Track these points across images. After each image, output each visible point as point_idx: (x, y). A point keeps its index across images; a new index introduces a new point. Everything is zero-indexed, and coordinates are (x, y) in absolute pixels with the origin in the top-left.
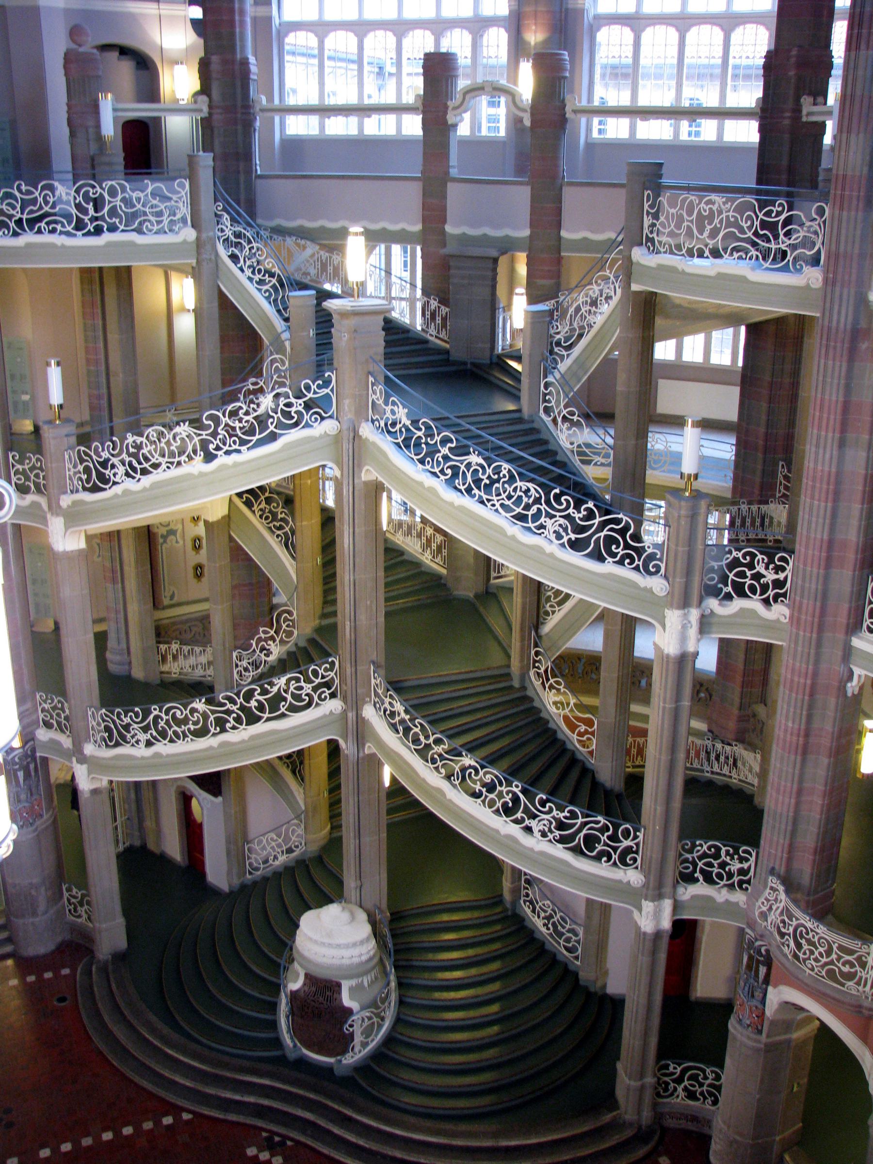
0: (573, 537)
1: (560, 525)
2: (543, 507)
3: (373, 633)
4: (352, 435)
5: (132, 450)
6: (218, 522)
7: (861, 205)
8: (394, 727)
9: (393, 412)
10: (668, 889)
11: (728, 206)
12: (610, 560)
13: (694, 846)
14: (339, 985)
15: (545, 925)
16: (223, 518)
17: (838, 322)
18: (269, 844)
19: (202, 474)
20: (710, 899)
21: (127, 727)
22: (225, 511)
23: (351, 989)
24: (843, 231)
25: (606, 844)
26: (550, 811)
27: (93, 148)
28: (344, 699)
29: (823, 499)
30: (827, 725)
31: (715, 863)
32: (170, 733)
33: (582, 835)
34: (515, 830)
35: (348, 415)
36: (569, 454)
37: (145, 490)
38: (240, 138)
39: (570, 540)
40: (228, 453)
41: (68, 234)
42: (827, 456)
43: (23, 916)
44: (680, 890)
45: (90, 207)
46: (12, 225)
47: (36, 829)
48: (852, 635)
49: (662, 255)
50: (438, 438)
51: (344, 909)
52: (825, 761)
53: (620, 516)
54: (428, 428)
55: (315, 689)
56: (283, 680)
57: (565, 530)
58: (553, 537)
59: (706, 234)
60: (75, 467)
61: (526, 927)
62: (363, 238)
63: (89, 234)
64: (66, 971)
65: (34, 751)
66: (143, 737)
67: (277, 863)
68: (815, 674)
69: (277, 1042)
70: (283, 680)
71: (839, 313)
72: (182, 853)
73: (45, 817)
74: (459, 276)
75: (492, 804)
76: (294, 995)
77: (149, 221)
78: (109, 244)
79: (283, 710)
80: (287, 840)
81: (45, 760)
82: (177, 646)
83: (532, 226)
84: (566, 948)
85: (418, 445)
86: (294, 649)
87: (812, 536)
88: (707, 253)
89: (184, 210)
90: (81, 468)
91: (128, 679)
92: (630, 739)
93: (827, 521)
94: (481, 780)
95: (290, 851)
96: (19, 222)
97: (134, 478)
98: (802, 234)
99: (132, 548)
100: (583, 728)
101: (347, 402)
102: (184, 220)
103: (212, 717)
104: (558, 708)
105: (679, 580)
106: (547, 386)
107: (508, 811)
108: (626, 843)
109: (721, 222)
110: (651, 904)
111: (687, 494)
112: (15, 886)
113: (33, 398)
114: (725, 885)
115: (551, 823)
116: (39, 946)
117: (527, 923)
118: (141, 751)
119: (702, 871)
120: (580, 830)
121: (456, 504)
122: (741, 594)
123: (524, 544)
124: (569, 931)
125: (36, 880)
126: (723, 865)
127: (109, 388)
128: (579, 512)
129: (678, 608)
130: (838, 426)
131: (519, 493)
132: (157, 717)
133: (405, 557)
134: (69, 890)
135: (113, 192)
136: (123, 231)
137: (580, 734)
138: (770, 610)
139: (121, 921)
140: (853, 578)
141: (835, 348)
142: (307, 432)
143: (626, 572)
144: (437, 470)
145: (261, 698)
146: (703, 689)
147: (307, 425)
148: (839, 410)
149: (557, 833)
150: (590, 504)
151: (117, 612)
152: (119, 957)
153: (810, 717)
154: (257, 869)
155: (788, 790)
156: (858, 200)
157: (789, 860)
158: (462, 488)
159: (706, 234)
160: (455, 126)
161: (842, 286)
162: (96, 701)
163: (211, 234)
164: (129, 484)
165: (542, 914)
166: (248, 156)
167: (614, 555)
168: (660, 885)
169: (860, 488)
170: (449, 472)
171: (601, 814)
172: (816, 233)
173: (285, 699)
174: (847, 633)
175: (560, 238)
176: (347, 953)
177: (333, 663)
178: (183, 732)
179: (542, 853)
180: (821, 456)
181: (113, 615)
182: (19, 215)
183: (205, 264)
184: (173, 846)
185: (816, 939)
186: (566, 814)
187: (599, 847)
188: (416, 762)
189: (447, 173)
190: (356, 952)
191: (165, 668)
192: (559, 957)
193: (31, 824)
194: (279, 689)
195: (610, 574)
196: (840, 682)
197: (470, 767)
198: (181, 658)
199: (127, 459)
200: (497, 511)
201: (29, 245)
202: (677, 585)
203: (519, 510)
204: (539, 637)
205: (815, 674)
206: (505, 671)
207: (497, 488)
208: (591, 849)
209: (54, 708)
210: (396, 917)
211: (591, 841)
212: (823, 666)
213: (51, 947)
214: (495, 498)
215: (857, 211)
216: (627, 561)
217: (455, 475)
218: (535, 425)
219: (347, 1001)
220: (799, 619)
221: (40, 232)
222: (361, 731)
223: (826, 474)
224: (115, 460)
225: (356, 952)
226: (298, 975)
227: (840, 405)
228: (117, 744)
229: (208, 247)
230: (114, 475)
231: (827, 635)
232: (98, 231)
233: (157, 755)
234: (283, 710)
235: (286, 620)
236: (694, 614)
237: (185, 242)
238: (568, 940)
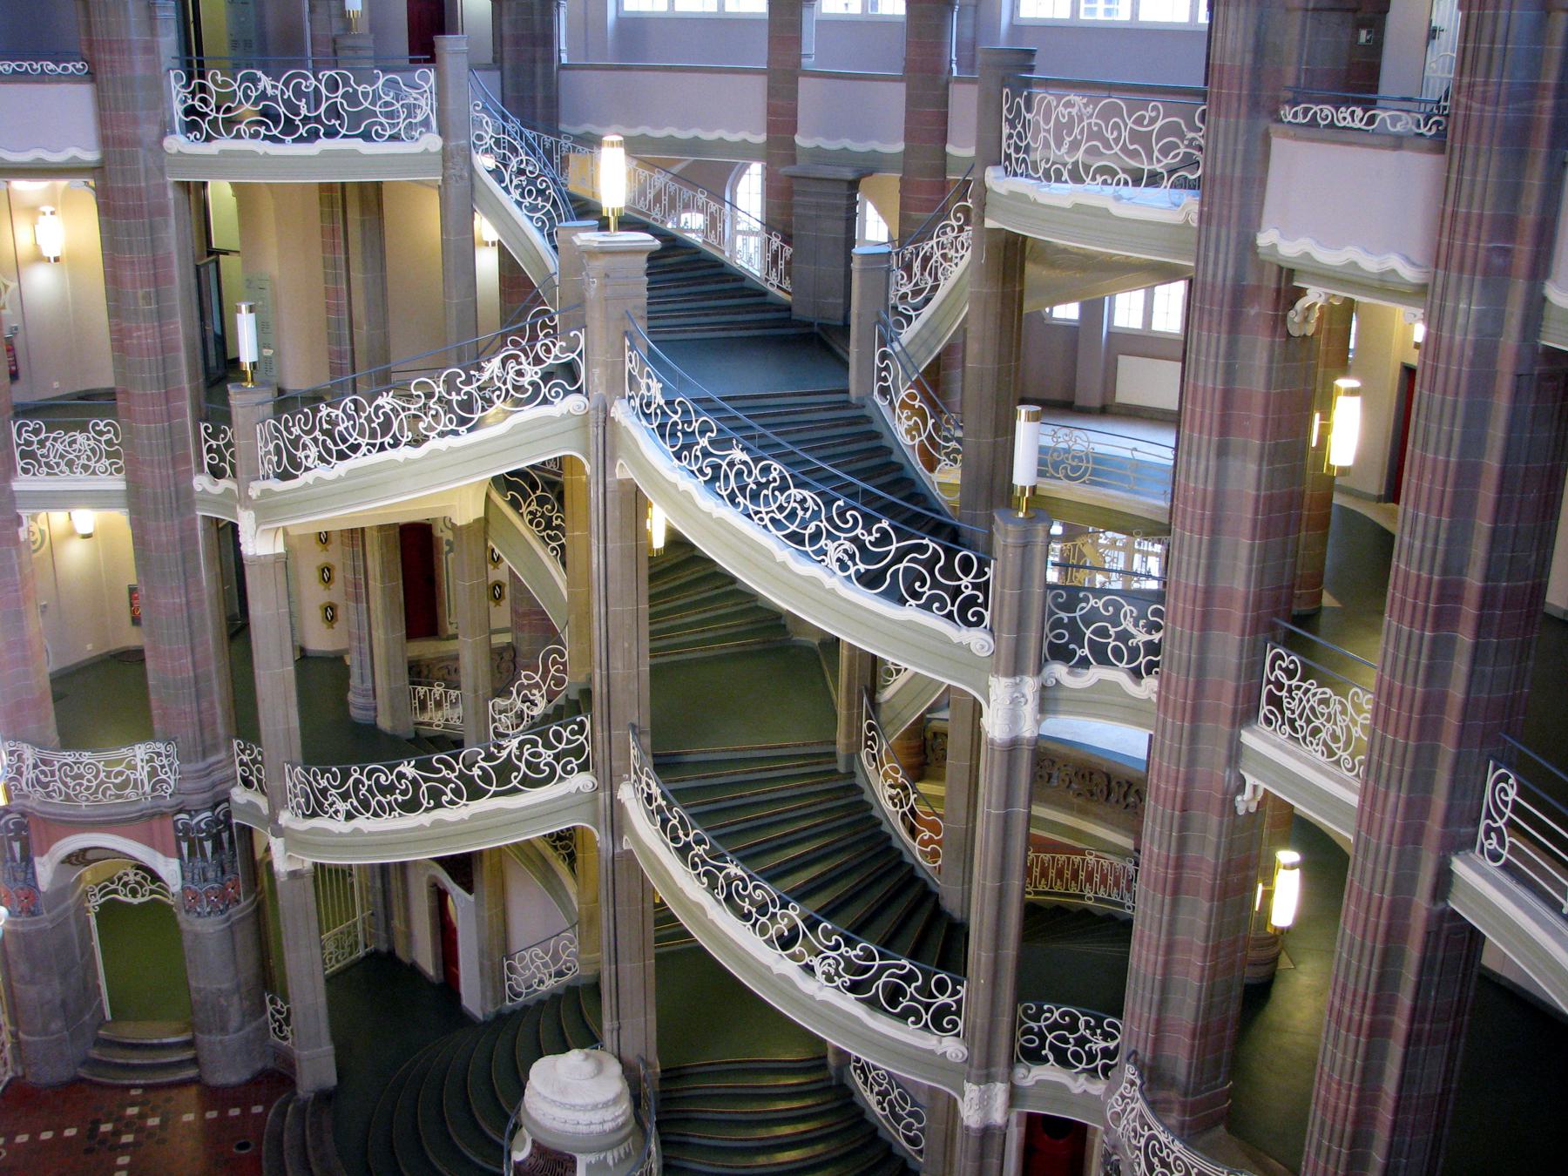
0: (862, 567)
1: (845, 551)
2: (824, 525)
3: (634, 686)
4: (601, 416)
5: (325, 426)
6: (468, 526)
7: (1244, 109)
9: (649, 389)
10: (1000, 1068)
11: (1090, 109)
12: (912, 602)
13: (1040, 1011)
14: (573, 1161)
15: (879, 1103)
16: (477, 521)
17: (1215, 276)
18: (532, 961)
19: (408, 462)
20: (1062, 1087)
21: (324, 792)
22: (479, 512)
23: (589, 1167)
24: (1220, 146)
25: (913, 999)
26: (837, 947)
27: (337, 27)
29: (1196, 528)
30: (1207, 853)
31: (1071, 1037)
32: (374, 803)
33: (880, 982)
34: (790, 968)
35: (598, 390)
36: (908, 452)
37: (339, 479)
38: (537, 18)
39: (858, 571)
40: (442, 434)
41: (274, 139)
42: (1202, 467)
43: (210, 1032)
44: (1020, 1071)
45: (303, 104)
46: (205, 126)
47: (228, 919)
48: (1241, 726)
49: (1019, 179)
50: (696, 425)
51: (587, 1056)
52: (1205, 905)
53: (925, 541)
54: (686, 412)
55: (557, 758)
57: (852, 557)
58: (835, 567)
59: (1064, 149)
60: (266, 445)
61: (854, 1104)
62: (622, 150)
63: (301, 139)
64: (257, 1109)
65: (228, 815)
66: (342, 806)
67: (543, 988)
68: (1189, 781)
71: (1216, 264)
72: (436, 967)
73: (243, 904)
74: (811, 204)
75: (763, 930)
76: (518, 1165)
77: (381, 124)
78: (325, 154)
79: (515, 782)
80: (556, 957)
81: (242, 827)
82: (441, 689)
83: (907, 139)
84: (907, 1138)
85: (673, 435)
86: (562, 703)
87: (1183, 581)
88: (1066, 176)
89: (427, 108)
90: (271, 447)
91: (372, 729)
92: (1031, 855)
93: (1203, 561)
94: (750, 896)
95: (560, 974)
96: (214, 123)
97: (329, 463)
98: (1182, 150)
99: (377, 555)
100: (927, 834)
101: (597, 371)
102: (426, 123)
103: (424, 787)
104: (895, 805)
105: (1007, 636)
106: (884, 356)
107: (786, 942)
108: (942, 999)
109: (1082, 131)
110: (975, 1087)
111: (1021, 515)
112: (199, 991)
113: (278, 354)
114: (1084, 1070)
115: (838, 964)
116: (229, 1074)
117: (856, 1098)
118: (340, 826)
119: (1053, 1047)
120: (878, 976)
121: (715, 515)
122: (1103, 660)
123: (797, 575)
124: (910, 1114)
125: (226, 986)
126: (1081, 1042)
127: (352, 343)
128: (870, 534)
129: (1006, 675)
130: (1216, 425)
131: (793, 504)
132: (357, 782)
133: (737, 586)
134: (273, 1001)
135: (333, 86)
136: (345, 136)
137: (924, 843)
138: (1139, 684)
139: (328, 1048)
140: (1242, 646)
141: (1211, 313)
142: (545, 410)
143: (933, 621)
144: (694, 468)
145: (484, 764)
146: (1133, 791)
147: (545, 401)
148: (1217, 404)
149: (847, 978)
150: (885, 524)
151: (360, 640)
152: (325, 1097)
153: (1182, 843)
154: (518, 995)
155: (1154, 942)
156: (1239, 100)
157: (1158, 1042)
158: (724, 494)
159: (1064, 149)
161: (1219, 226)
162: (297, 754)
163: (463, 142)
164: (323, 471)
165: (876, 1089)
166: (547, 39)
167: (916, 595)
168: (988, 1062)
169: (1249, 515)
170: (708, 471)
171: (903, 955)
172: (1200, 149)
173: (518, 770)
174: (1233, 725)
175: (945, 154)
176: (584, 1117)
177: (582, 725)
178: (389, 803)
179: (825, 1003)
180: (1193, 468)
181: (355, 643)
182: (214, 114)
183: (452, 182)
184: (425, 957)
185: (1171, 1160)
186: (858, 952)
187: (905, 1003)
189: (799, 64)
190: (596, 1117)
191: (425, 718)
192: (896, 1150)
193: (222, 912)
194: (509, 754)
195: (910, 621)
196: (1225, 793)
198: (446, 706)
199: (321, 438)
200: (765, 527)
201: (224, 153)
202: (1003, 644)
203: (793, 528)
204: (874, 704)
205: (1189, 781)
206: (830, 749)
207: (766, 496)
208: (893, 1002)
209: (254, 761)
210: (671, 1075)
211: (894, 994)
212: (1201, 769)
213: (245, 1075)
214: (763, 509)
215: (1238, 116)
216: (936, 605)
217: (715, 478)
218: (866, 412)
220: (1167, 699)
221: (238, 136)
222: (616, 821)
223: (1200, 494)
224: (306, 439)
225: (596, 1117)
226: (524, 1141)
227: (1218, 396)
228: (314, 815)
229: (459, 159)
230: (307, 457)
231: (1207, 725)
232: (313, 136)
233: (357, 831)
234: (515, 782)
235: (555, 662)
236: (1030, 685)
237: (426, 152)
238: (909, 1127)
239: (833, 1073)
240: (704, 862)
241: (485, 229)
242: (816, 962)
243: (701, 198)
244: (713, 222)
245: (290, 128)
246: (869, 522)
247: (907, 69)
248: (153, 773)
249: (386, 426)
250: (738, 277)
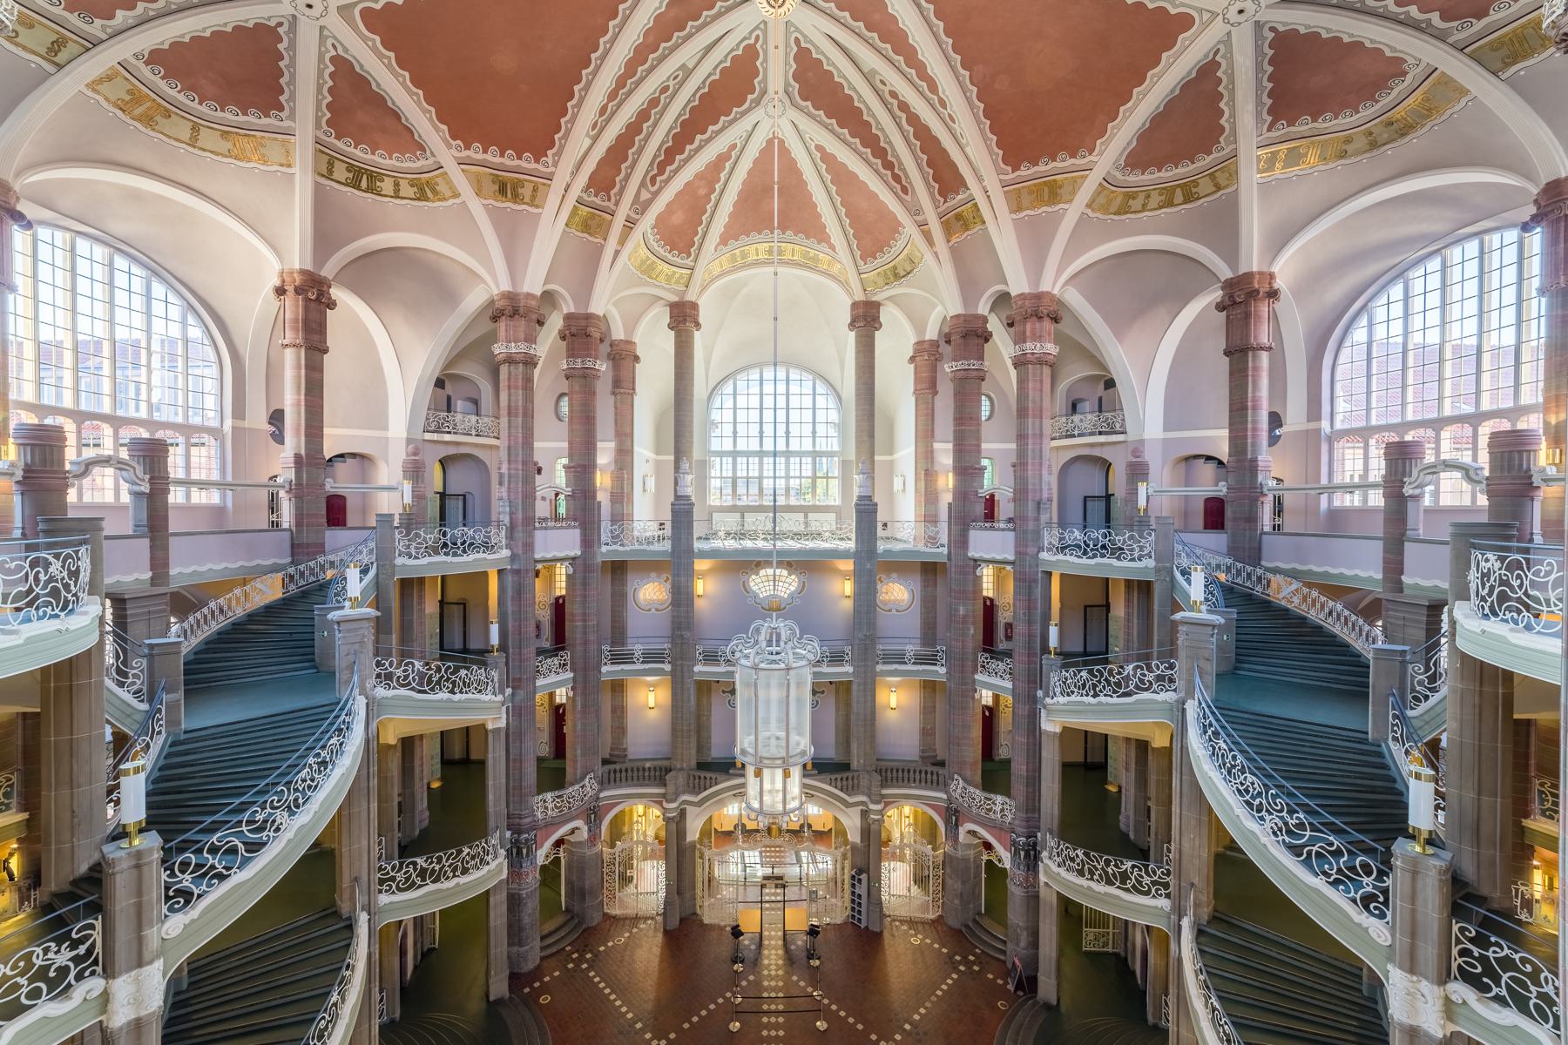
56: (1130, 864)
70: (1130, 864)
142: (1154, 696)
160: (1417, 498)
232: (1095, 556)
245: (1085, 553)
246: (1291, 812)
247: (1454, 535)
249: (1084, 686)
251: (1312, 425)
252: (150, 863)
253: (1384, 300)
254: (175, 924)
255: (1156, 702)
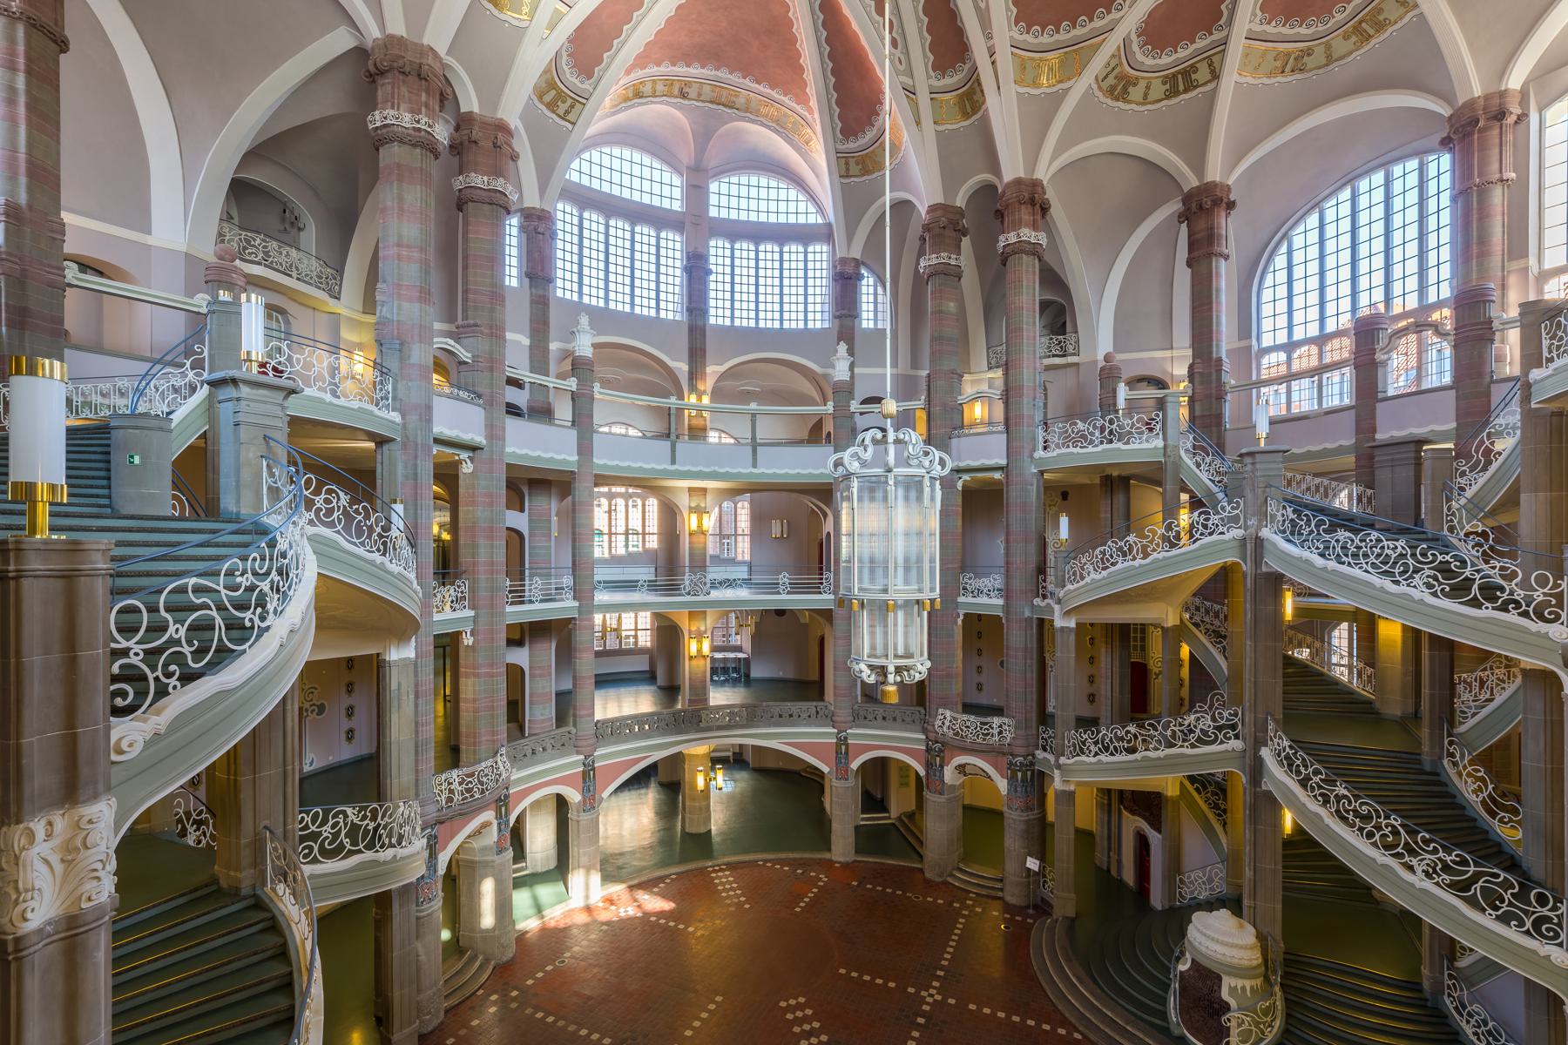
8: (1281, 763)
26: (1435, 851)
28: (1244, 740)
57: (1436, 579)
65: (1032, 764)
69: (1164, 1015)
108: (1545, 911)
135: (1111, 422)
188: (1314, 807)
197: (1345, 797)
219: (1225, 994)
222: (1257, 770)
239: (1428, 996)
240: (1320, 787)
241: (1185, 651)
242: (1414, 862)
243: (1309, 639)
244: (1315, 653)
248: (1000, 733)
250: (1336, 682)
251: (1243, 343)
252: (93, 575)
253: (1301, 228)
254: (131, 734)
255: (1225, 542)
